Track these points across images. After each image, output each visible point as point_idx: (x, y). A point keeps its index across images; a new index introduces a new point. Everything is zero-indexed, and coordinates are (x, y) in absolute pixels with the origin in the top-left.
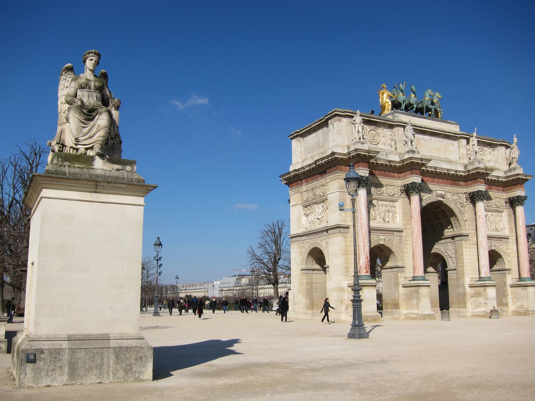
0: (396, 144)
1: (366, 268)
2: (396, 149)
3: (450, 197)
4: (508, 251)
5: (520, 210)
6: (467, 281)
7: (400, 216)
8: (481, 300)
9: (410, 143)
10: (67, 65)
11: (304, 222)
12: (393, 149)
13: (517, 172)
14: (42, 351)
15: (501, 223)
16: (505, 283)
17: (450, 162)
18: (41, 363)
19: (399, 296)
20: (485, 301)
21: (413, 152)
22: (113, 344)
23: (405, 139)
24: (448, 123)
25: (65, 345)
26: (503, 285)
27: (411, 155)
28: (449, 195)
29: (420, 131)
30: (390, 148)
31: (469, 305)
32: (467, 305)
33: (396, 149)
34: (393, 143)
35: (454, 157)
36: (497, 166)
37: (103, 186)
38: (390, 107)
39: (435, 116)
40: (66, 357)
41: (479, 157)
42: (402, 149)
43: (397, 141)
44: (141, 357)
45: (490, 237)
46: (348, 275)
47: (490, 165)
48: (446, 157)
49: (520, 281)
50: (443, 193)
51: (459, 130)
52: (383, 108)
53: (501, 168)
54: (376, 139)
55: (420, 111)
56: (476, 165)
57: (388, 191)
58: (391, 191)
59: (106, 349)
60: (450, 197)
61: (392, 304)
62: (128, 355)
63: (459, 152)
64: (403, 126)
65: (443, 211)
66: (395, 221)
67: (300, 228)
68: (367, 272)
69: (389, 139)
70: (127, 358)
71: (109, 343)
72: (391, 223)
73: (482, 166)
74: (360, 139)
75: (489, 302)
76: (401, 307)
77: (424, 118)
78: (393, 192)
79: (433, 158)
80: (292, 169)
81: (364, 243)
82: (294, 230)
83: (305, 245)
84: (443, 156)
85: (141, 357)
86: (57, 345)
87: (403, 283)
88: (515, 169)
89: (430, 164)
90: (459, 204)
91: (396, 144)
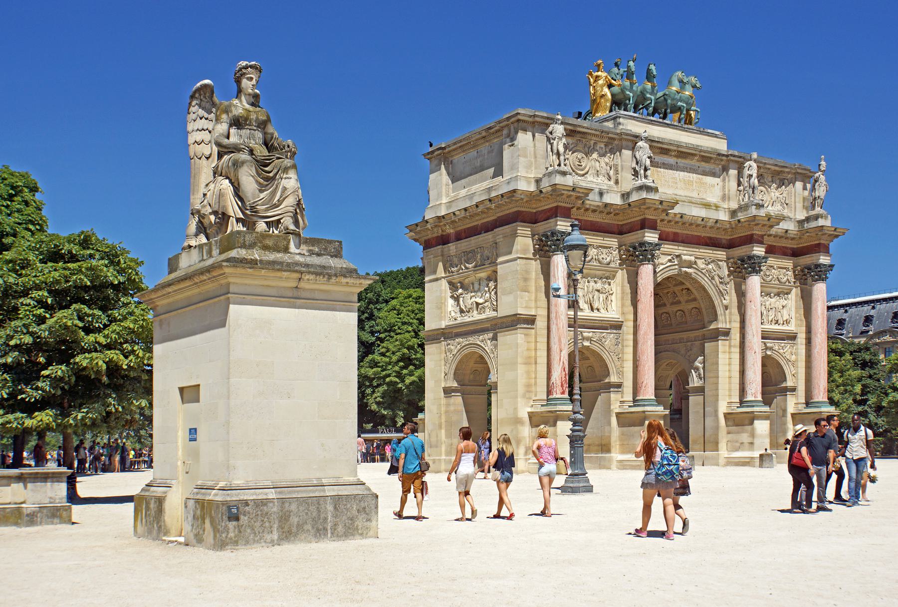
0: (617, 172)
1: (562, 386)
2: (617, 182)
3: (703, 266)
4: (793, 357)
5: (820, 290)
6: (723, 408)
7: (617, 301)
8: (745, 437)
9: (642, 172)
10: (198, 85)
11: (450, 309)
12: (612, 183)
13: (821, 222)
14: (246, 503)
15: (785, 312)
16: (785, 411)
17: (707, 206)
18: (246, 518)
19: (610, 432)
20: (750, 440)
21: (649, 189)
22: (330, 492)
23: (634, 165)
24: (708, 134)
25: (272, 494)
26: (780, 413)
27: (644, 195)
28: (701, 264)
29: (660, 148)
30: (606, 181)
31: (723, 445)
32: (720, 445)
33: (617, 182)
34: (612, 173)
35: (713, 197)
36: (786, 212)
37: (308, 280)
38: (608, 104)
39: (687, 122)
40: (275, 508)
41: (758, 198)
42: (628, 182)
43: (620, 168)
44: (364, 508)
45: (765, 336)
46: (530, 398)
47: (773, 210)
48: (701, 196)
49: (741, 407)
50: (692, 258)
51: (726, 149)
52: (595, 104)
53: (792, 216)
54: (583, 164)
55: (662, 111)
56: (753, 211)
57: (600, 257)
58: (604, 256)
59: (322, 499)
60: (703, 266)
61: (598, 445)
62: (349, 506)
63: (724, 187)
64: (633, 141)
65: (688, 289)
66: (609, 306)
67: (441, 319)
68: (563, 393)
69: (607, 164)
70: (347, 510)
71: (324, 491)
72: (602, 310)
73: (762, 212)
74: (559, 165)
75: (757, 442)
76: (613, 450)
77: (668, 125)
78: (608, 259)
79: (678, 198)
80: (429, 215)
81: (560, 345)
82: (431, 323)
83: (452, 347)
84: (694, 194)
85: (364, 508)
86: (260, 495)
87: (617, 411)
88: (816, 217)
89: (677, 210)
90: (716, 278)
91: (617, 172)
